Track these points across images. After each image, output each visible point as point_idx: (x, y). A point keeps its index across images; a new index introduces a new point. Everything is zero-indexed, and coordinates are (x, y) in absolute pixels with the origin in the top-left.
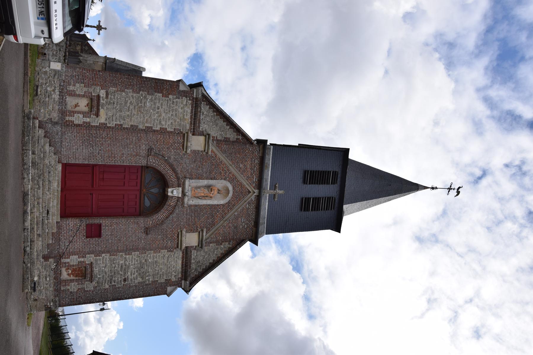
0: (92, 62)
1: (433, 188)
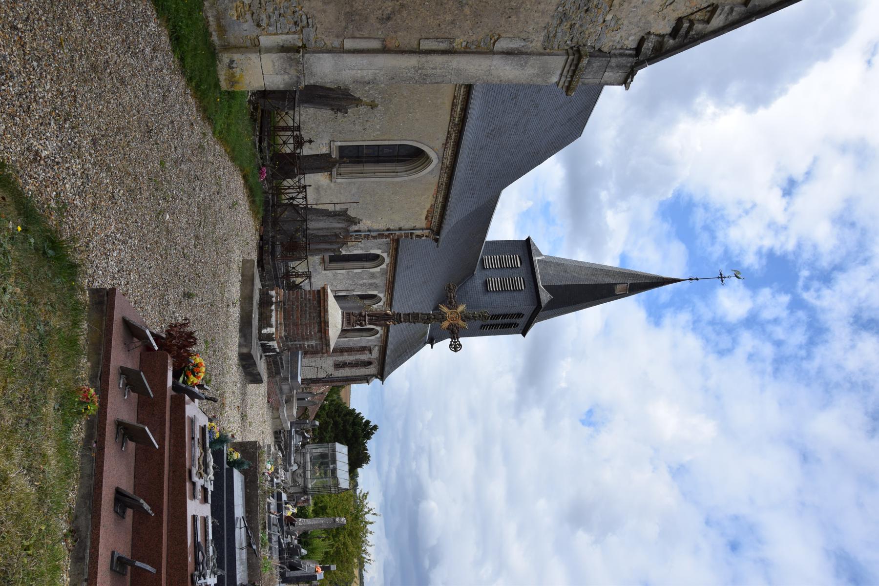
1: (691, 279)
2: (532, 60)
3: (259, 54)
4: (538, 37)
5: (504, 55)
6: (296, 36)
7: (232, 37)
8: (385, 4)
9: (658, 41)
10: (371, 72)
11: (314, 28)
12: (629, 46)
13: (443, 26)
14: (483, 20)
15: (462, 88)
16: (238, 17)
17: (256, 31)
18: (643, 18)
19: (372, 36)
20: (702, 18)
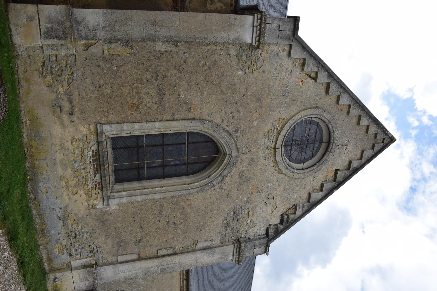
2: (217, 250)
3: (71, 271)
4: (217, 238)
5: (202, 251)
6: (92, 258)
7: (55, 265)
8: (137, 235)
9: (275, 228)
10: (134, 272)
11: (101, 253)
12: (263, 233)
13: (168, 241)
14: (188, 235)
15: (184, 281)
16: (59, 252)
17: (70, 259)
18: (265, 218)
19: (132, 252)
20: (291, 212)
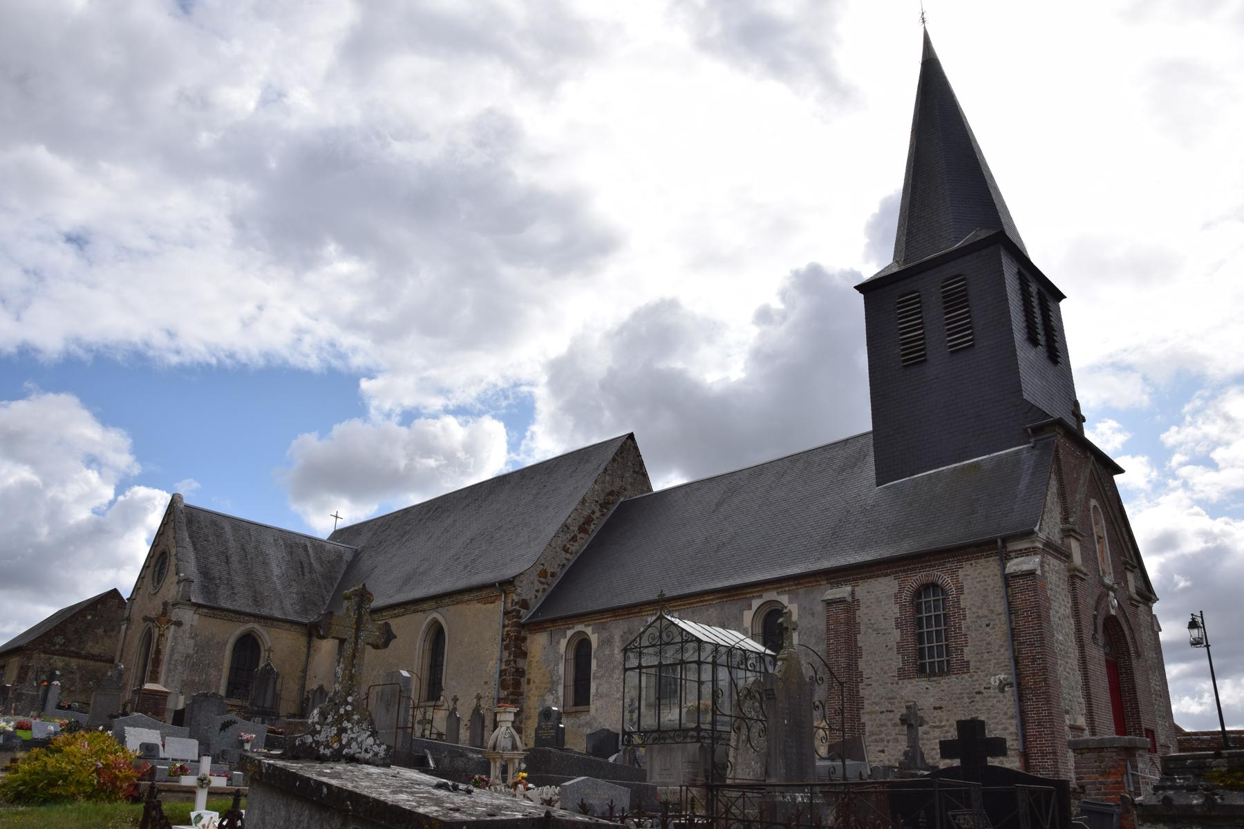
0: (192, 642)
1: (924, 22)
